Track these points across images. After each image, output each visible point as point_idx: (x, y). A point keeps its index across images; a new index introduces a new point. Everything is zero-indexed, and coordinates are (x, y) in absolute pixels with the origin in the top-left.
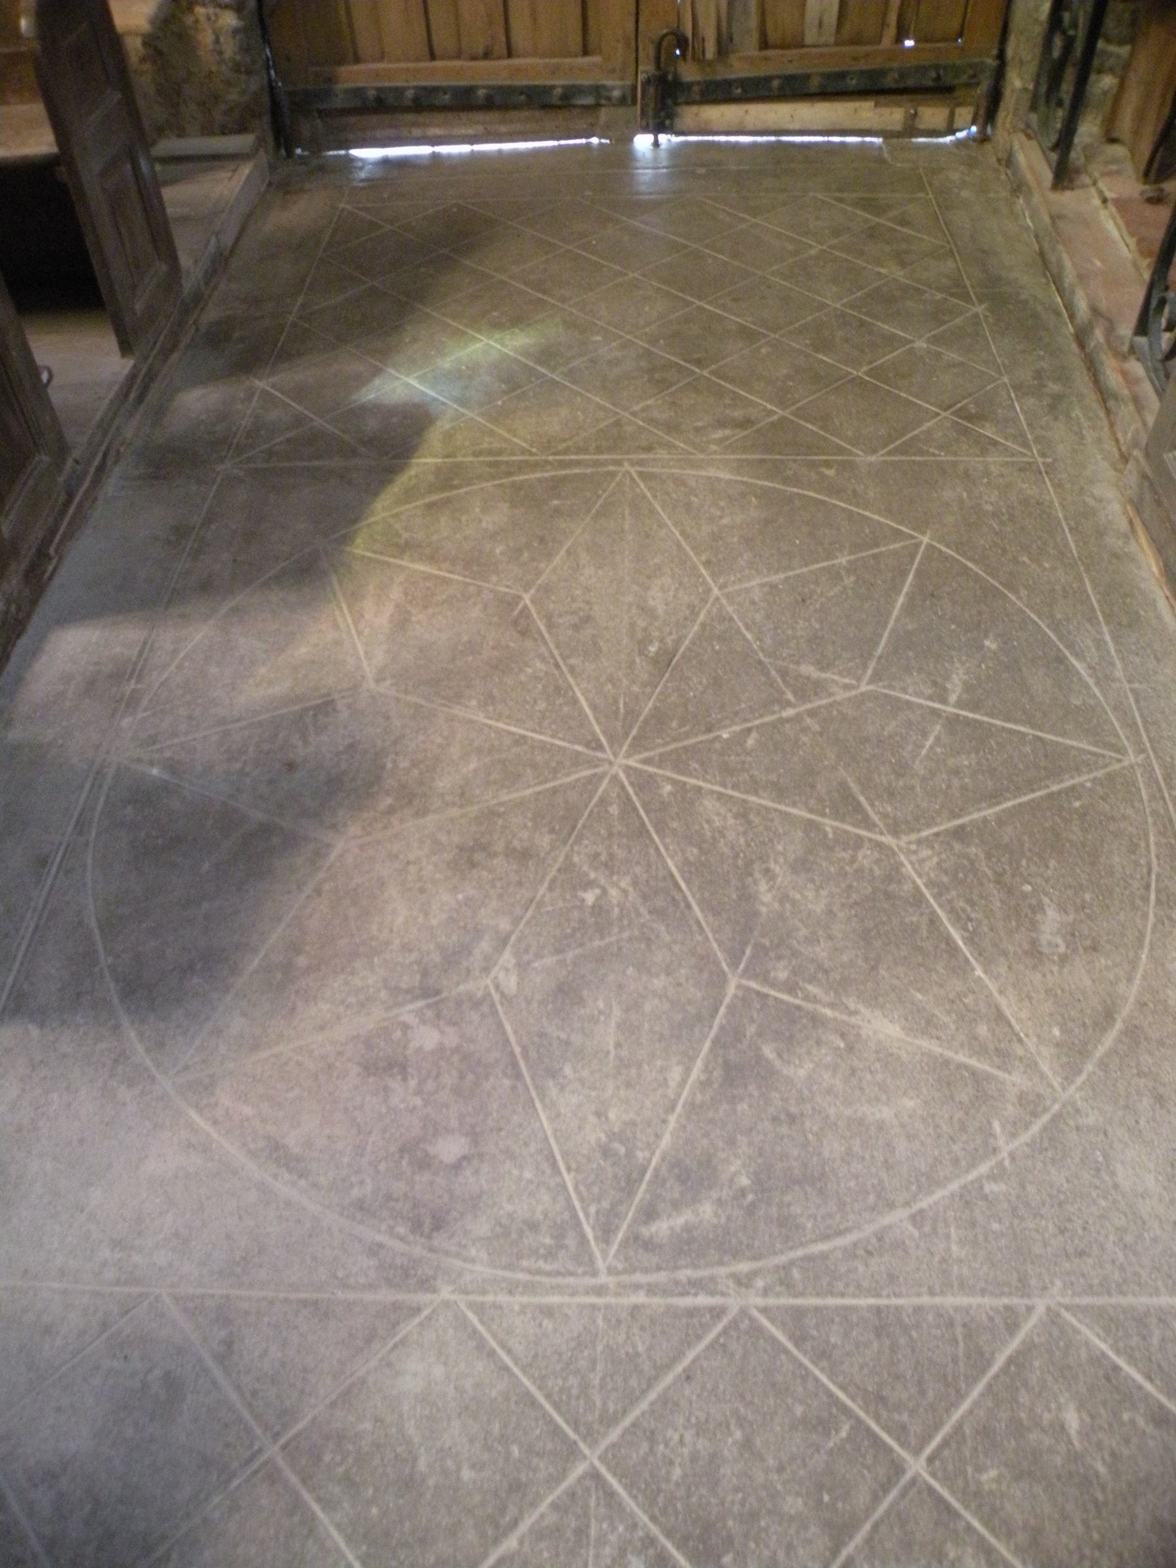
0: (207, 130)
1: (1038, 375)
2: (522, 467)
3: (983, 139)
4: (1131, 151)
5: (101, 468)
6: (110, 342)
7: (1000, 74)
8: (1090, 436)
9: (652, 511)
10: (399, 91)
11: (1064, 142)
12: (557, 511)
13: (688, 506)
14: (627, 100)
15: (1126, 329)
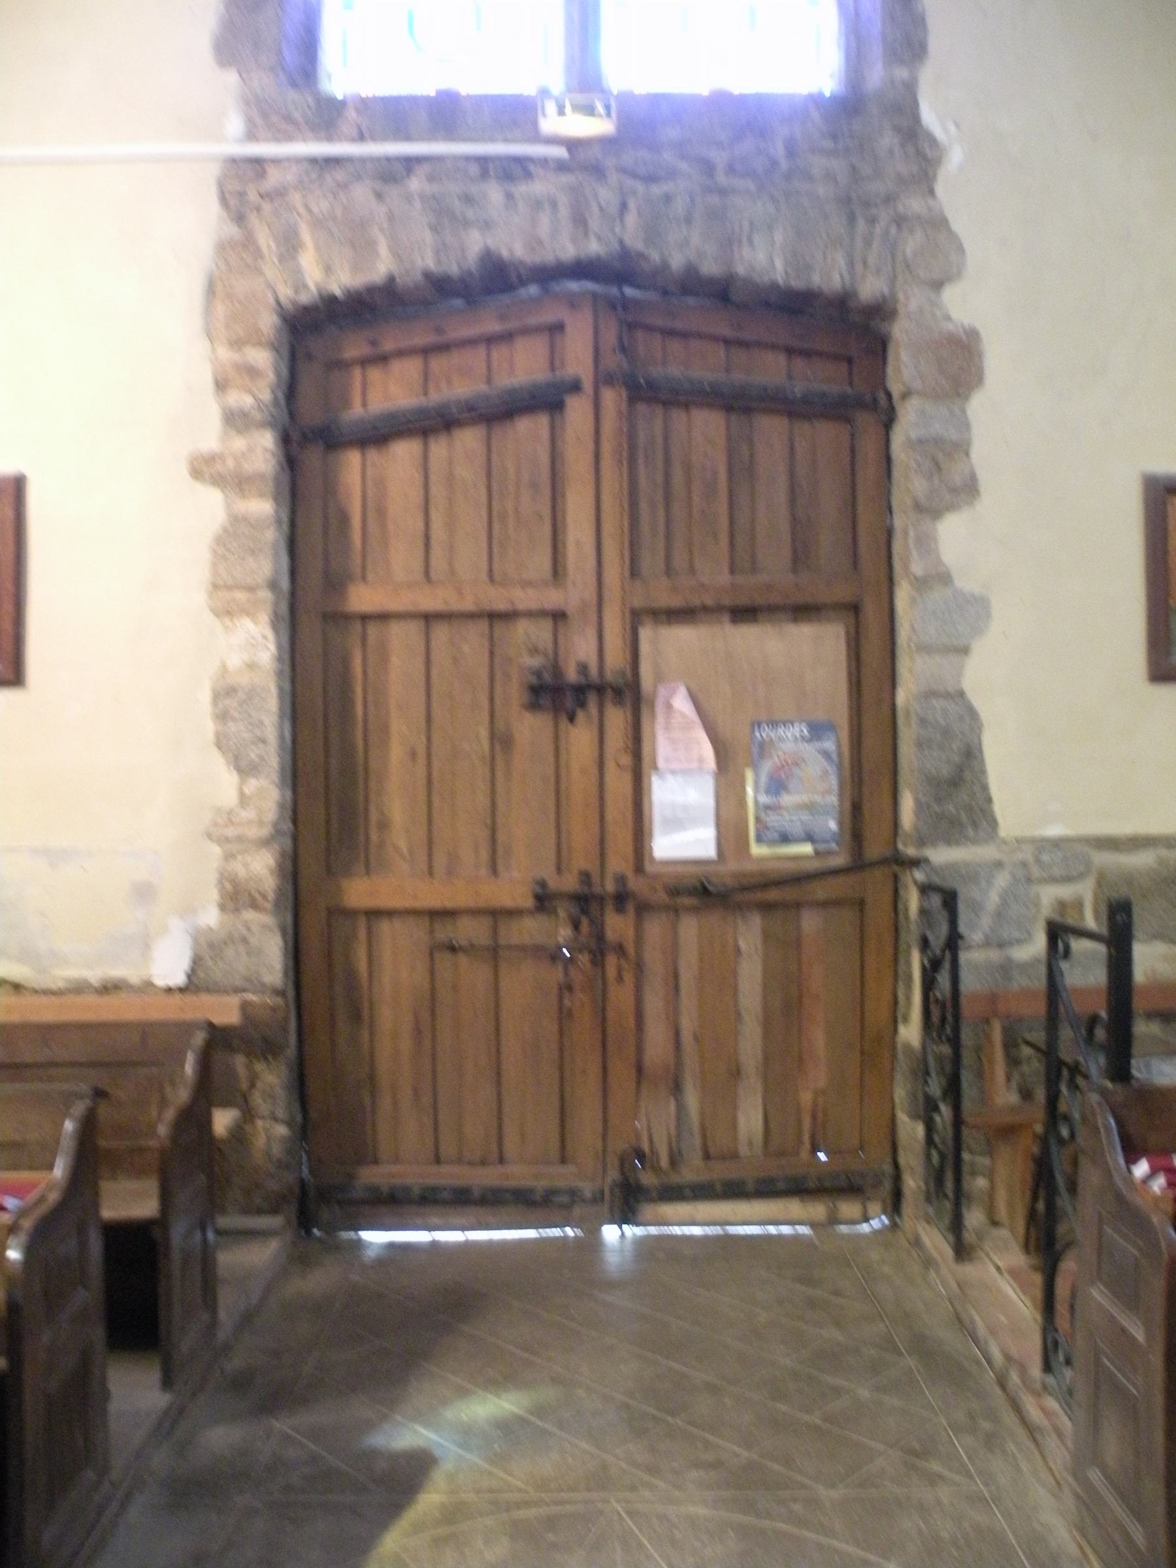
0: (246, 1211)
1: (972, 1416)
2: (519, 1506)
3: (894, 1226)
4: (1012, 1232)
5: (128, 1496)
6: (154, 1375)
7: (897, 1178)
8: (1025, 1467)
9: (640, 1545)
10: (407, 1189)
11: (956, 1226)
12: (554, 1546)
13: (673, 1542)
14: (598, 1198)
15: (1035, 1371)
